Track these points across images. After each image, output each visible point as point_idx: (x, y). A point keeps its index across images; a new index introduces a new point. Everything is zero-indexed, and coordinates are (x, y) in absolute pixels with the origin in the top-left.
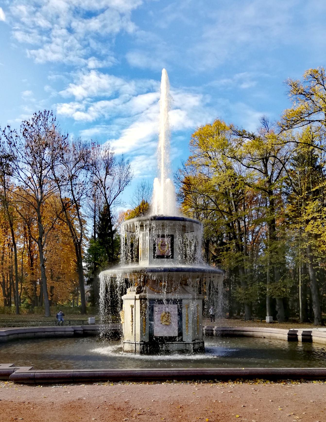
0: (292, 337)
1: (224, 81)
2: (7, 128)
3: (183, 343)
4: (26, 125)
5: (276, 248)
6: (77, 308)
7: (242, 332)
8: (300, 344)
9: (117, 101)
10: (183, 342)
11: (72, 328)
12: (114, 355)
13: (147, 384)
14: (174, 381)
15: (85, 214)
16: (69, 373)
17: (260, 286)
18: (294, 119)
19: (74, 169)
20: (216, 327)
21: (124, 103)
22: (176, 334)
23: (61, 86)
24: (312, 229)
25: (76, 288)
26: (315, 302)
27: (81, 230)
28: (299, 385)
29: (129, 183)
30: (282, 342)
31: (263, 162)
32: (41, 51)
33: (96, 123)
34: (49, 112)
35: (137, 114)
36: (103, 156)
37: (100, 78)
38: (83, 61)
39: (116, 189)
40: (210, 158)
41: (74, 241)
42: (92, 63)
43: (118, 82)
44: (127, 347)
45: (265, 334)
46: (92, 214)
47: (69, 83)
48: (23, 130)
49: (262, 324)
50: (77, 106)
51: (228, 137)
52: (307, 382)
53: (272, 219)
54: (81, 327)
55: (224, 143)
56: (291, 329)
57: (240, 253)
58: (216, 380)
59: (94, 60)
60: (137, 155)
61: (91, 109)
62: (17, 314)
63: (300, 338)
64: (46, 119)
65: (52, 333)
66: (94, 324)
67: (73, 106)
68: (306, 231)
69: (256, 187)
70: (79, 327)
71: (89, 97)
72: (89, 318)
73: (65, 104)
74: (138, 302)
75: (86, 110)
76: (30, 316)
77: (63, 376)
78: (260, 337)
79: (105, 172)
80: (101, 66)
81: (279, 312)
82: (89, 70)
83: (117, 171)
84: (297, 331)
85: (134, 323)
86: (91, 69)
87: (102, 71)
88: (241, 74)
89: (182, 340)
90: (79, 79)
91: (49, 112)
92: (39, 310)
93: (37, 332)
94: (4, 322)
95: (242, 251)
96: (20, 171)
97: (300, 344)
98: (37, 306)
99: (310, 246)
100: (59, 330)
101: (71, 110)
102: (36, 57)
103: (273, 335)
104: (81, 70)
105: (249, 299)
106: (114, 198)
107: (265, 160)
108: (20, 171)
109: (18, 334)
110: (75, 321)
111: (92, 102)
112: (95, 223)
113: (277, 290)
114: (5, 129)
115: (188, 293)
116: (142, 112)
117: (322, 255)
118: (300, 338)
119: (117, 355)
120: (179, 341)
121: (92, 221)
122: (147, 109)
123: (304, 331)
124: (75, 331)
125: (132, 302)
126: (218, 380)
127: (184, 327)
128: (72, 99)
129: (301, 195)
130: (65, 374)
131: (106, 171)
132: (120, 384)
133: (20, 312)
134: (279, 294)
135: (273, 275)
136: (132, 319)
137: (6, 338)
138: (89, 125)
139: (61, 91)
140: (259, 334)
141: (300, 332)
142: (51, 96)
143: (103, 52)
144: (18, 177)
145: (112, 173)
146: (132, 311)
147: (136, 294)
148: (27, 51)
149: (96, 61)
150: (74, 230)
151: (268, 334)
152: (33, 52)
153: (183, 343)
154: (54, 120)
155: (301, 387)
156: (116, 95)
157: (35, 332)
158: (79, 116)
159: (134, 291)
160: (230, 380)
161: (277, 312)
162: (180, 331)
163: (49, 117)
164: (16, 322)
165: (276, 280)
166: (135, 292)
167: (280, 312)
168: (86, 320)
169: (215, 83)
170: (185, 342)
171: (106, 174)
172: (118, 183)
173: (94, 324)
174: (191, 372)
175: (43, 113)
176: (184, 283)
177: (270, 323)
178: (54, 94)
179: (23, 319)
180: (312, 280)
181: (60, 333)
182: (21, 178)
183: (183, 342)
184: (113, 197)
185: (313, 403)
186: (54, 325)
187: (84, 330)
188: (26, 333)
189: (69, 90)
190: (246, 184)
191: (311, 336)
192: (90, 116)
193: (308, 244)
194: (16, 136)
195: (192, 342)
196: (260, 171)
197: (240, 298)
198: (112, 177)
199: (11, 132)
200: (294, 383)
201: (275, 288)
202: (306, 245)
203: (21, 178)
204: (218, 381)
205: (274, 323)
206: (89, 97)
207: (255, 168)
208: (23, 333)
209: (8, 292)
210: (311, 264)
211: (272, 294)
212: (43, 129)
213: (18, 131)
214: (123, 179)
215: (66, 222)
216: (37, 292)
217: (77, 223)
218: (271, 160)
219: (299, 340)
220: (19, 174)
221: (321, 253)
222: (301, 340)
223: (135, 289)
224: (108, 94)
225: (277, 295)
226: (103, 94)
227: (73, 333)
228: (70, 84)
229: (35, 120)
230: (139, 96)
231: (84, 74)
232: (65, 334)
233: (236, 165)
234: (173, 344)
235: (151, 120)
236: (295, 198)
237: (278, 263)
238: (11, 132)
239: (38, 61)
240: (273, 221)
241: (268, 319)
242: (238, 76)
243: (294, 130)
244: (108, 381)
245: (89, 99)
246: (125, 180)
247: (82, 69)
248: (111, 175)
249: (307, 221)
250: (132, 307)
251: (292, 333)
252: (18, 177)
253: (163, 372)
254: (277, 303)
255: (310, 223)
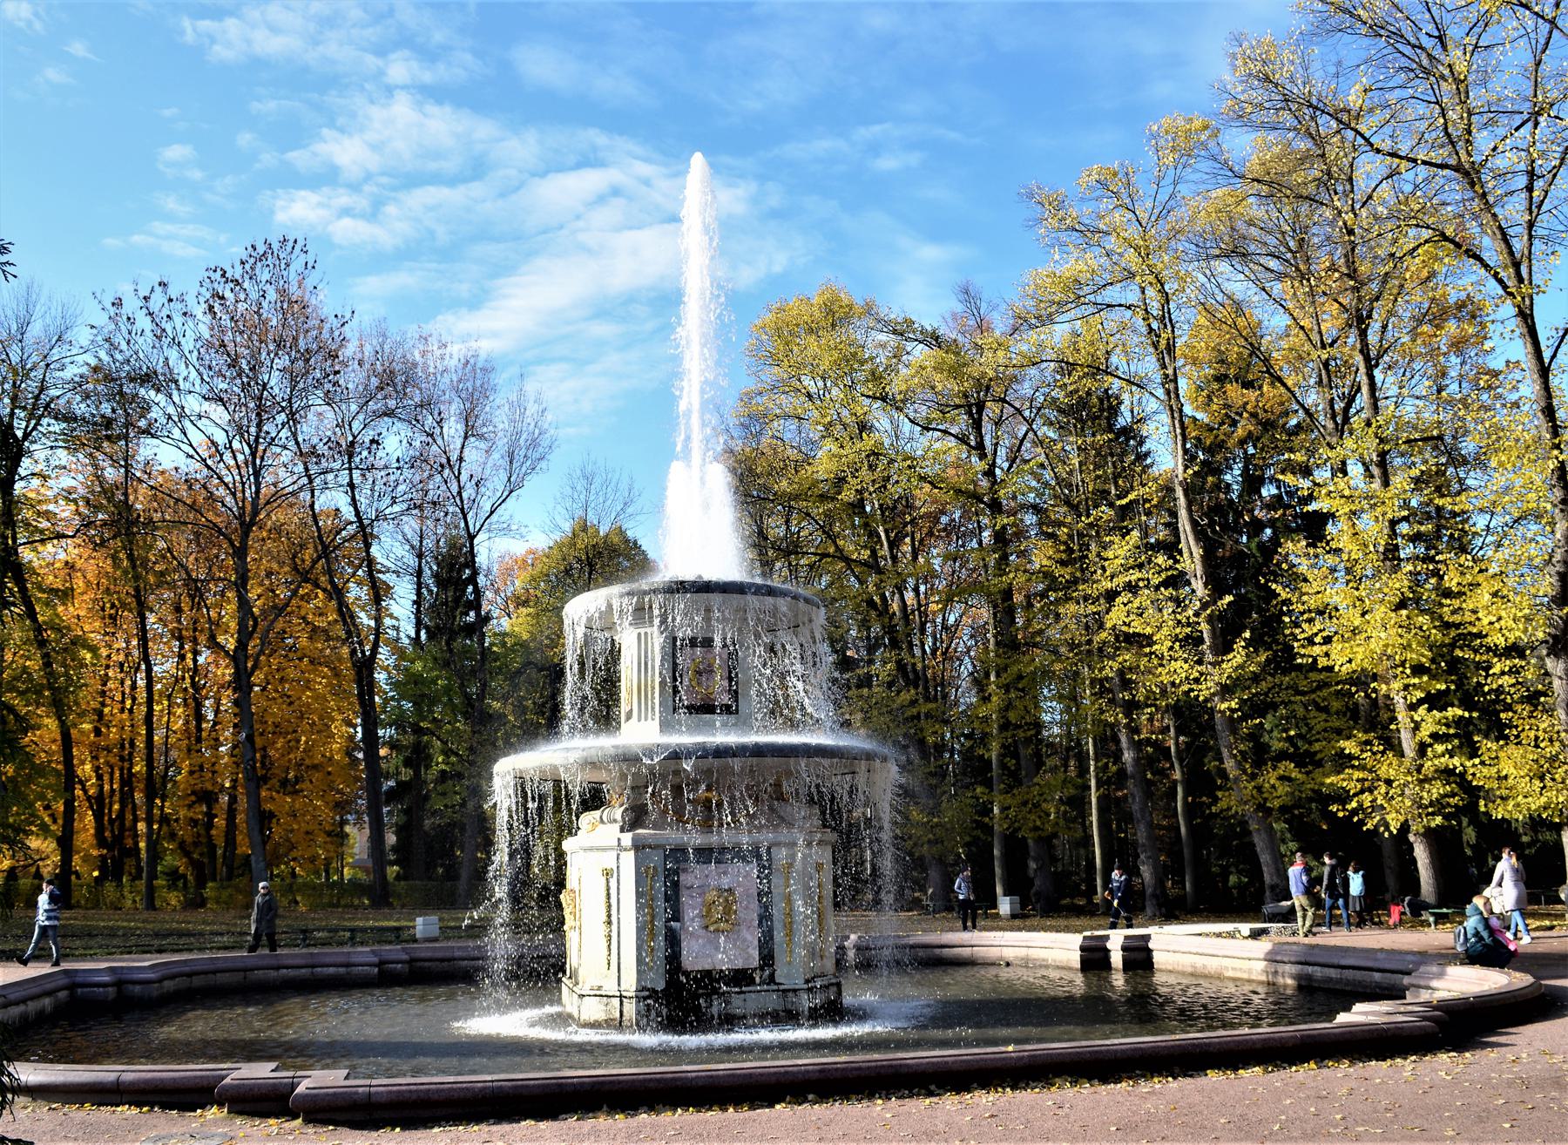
0: (1094, 958)
1: (823, 145)
2: (158, 289)
3: (778, 990)
4: (219, 279)
5: (1020, 677)
6: (356, 887)
7: (937, 951)
8: (1118, 980)
9: (476, 189)
10: (775, 987)
11: (373, 952)
13: (731, 1110)
14: (810, 1097)
15: (390, 565)
16: (479, 1085)
17: (978, 799)
18: (1057, 299)
19: (361, 417)
20: (853, 937)
21: (503, 195)
22: (755, 962)
23: (293, 134)
24: (1127, 620)
25: (338, 818)
26: (1144, 845)
27: (378, 620)
28: (1173, 1085)
29: (543, 464)
30: (1064, 974)
31: (970, 414)
32: (231, 24)
33: (405, 255)
34: (296, 241)
35: (544, 232)
36: (455, 379)
37: (425, 115)
38: (371, 61)
39: (497, 484)
40: (809, 396)
41: (353, 652)
42: (399, 69)
43: (484, 129)
44: (593, 1010)
45: (1009, 954)
46: (412, 561)
47: (320, 127)
48: (208, 295)
49: (989, 923)
50: (344, 199)
51: (859, 336)
52: (1191, 1076)
53: (1005, 586)
54: (403, 949)
55: (854, 355)
56: (1088, 933)
57: (913, 691)
58: (933, 1087)
59: (407, 60)
60: (541, 361)
61: (391, 209)
62: (147, 909)
63: (1117, 958)
64: (283, 262)
65: (303, 971)
66: (435, 940)
67: (330, 198)
68: (1109, 625)
69: (952, 488)
70: (393, 951)
71: (383, 174)
72: (419, 920)
73: (303, 193)
74: (629, 859)
75: (373, 214)
76: (189, 916)
77: (462, 1094)
78: (993, 964)
79: (461, 427)
80: (427, 77)
81: (1037, 882)
82: (389, 90)
83: (501, 426)
84: (1107, 938)
85: (614, 927)
86: (397, 87)
87: (430, 94)
88: (876, 129)
89: (771, 979)
90: (353, 115)
91: (296, 241)
92: (225, 894)
93: (252, 970)
94: (115, 936)
95: (916, 687)
96: (187, 424)
97: (1118, 980)
98: (214, 880)
99: (1121, 673)
100: (328, 960)
101: (322, 212)
102: (213, 40)
103: (1035, 954)
104: (363, 89)
105: (942, 842)
106: (492, 513)
107: (975, 410)
108: (187, 424)
109: (190, 975)
110: (364, 930)
111: (395, 189)
112: (419, 594)
113: (1030, 812)
114: (152, 290)
115: (790, 825)
116: (561, 227)
117: (1156, 699)
118: (1117, 958)
121: (410, 586)
122: (578, 217)
123: (1126, 938)
124: (381, 964)
125: (609, 860)
126: (939, 1087)
127: (779, 936)
128: (327, 177)
129: (1088, 516)
130: (467, 1089)
131: (467, 426)
132: (644, 1116)
133: (158, 903)
134: (1038, 823)
135: (1014, 761)
136: (609, 916)
137: (155, 990)
138: (380, 261)
139: (293, 149)
140: (993, 953)
141: (1116, 940)
142: (257, 165)
143: (438, 37)
144: (180, 444)
145: (485, 430)
147: (622, 830)
148: (186, 23)
149: (414, 64)
150: (352, 617)
151: (1022, 952)
152: (206, 25)
153: (778, 990)
154: (309, 266)
155: (1181, 1089)
156: (477, 169)
157: (245, 970)
158: (347, 230)
159: (615, 821)
160: (975, 1085)
162: (766, 952)
163: (293, 256)
164: (157, 935)
165: (1025, 780)
166: (617, 827)
168: (409, 928)
169: (792, 150)
170: (782, 987)
171: (466, 434)
172: (505, 463)
173: (435, 940)
174: (860, 1069)
175: (275, 246)
176: (773, 800)
177: (1014, 916)
178: (268, 159)
179: (175, 925)
180: (1133, 777)
181: (332, 970)
182: (191, 445)
183: (775, 987)
184: (487, 507)
185: (1227, 1126)
186: (298, 946)
187: (412, 961)
188: (214, 972)
189: (320, 148)
190: (922, 478)
191: (1149, 951)
192: (385, 234)
193: (1116, 666)
194: (185, 314)
195: (806, 986)
196: (962, 439)
197: (914, 839)
198: (483, 445)
199: (170, 300)
200: (1156, 1080)
201: (1025, 803)
202: (1111, 668)
203: (191, 445)
204: (941, 1091)
205: (1024, 917)
206: (383, 174)
207: (945, 432)
208: (205, 973)
209: (112, 831)
210: (1127, 726)
211: (1016, 825)
212: (272, 295)
213: (191, 300)
214: (522, 453)
215: (324, 590)
216: (213, 832)
217: (356, 593)
218: (992, 409)
219: (1113, 965)
220: (185, 434)
221: (1154, 693)
222: (1121, 966)
223: (619, 817)
224: (450, 166)
225: (1031, 825)
226: (432, 166)
227: (376, 970)
228: (325, 131)
229: (247, 267)
230: (550, 176)
231: (372, 102)
232: (348, 973)
233: (882, 420)
234: (744, 992)
235: (589, 251)
237: (1030, 724)
238: (170, 300)
239: (220, 52)
240: (1007, 594)
241: (1005, 906)
242: (864, 133)
243: (1056, 327)
244: (605, 1108)
245: (384, 180)
246: (529, 454)
247: (367, 86)
248: (481, 437)
249: (1111, 596)
250: (608, 874)
251: (1093, 943)
252: (180, 444)
253: (775, 1073)
254: (1032, 854)
255: (1119, 600)
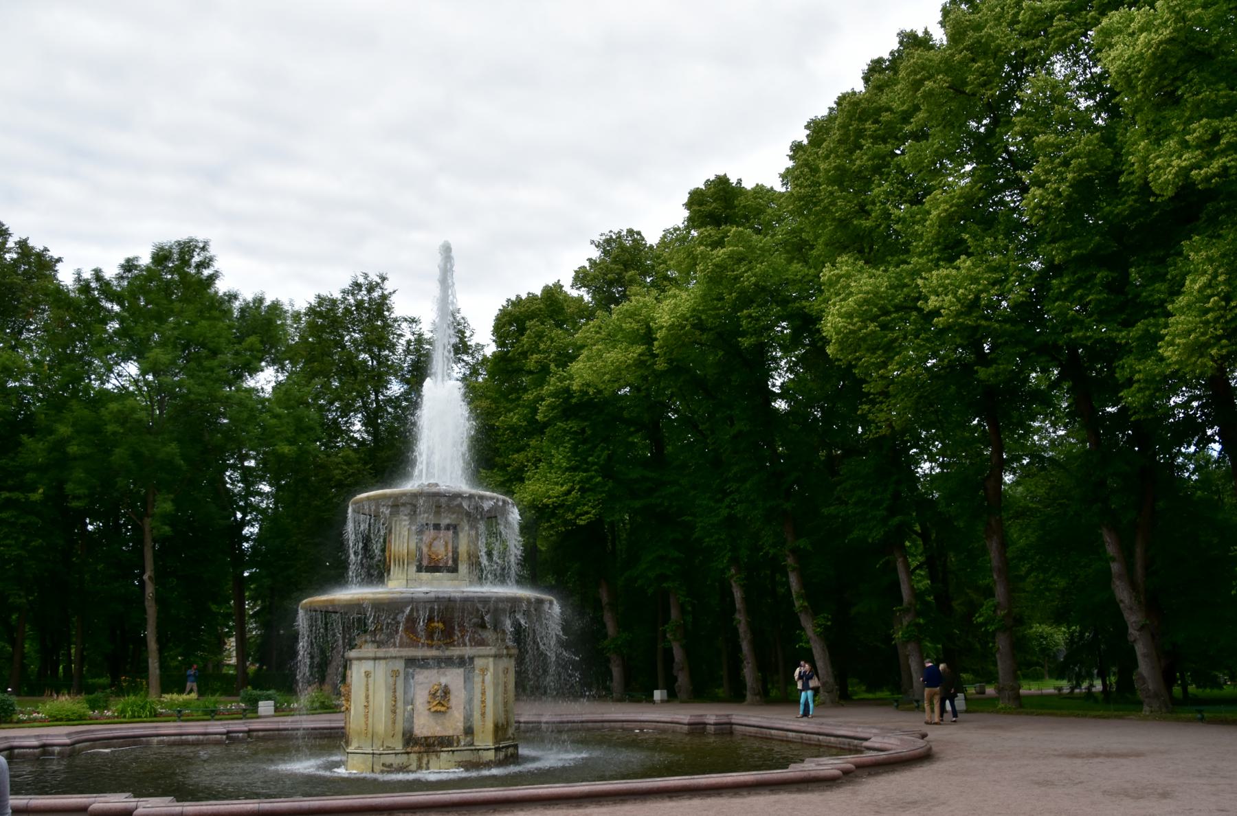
12: (322, 773)
81: (679, 679)
119: (328, 774)
120: (464, 745)
146: (367, 685)
161: (676, 679)
167: (683, 679)
177: (662, 701)
187: (228, 732)
236: (1221, 116)
241: (658, 695)
